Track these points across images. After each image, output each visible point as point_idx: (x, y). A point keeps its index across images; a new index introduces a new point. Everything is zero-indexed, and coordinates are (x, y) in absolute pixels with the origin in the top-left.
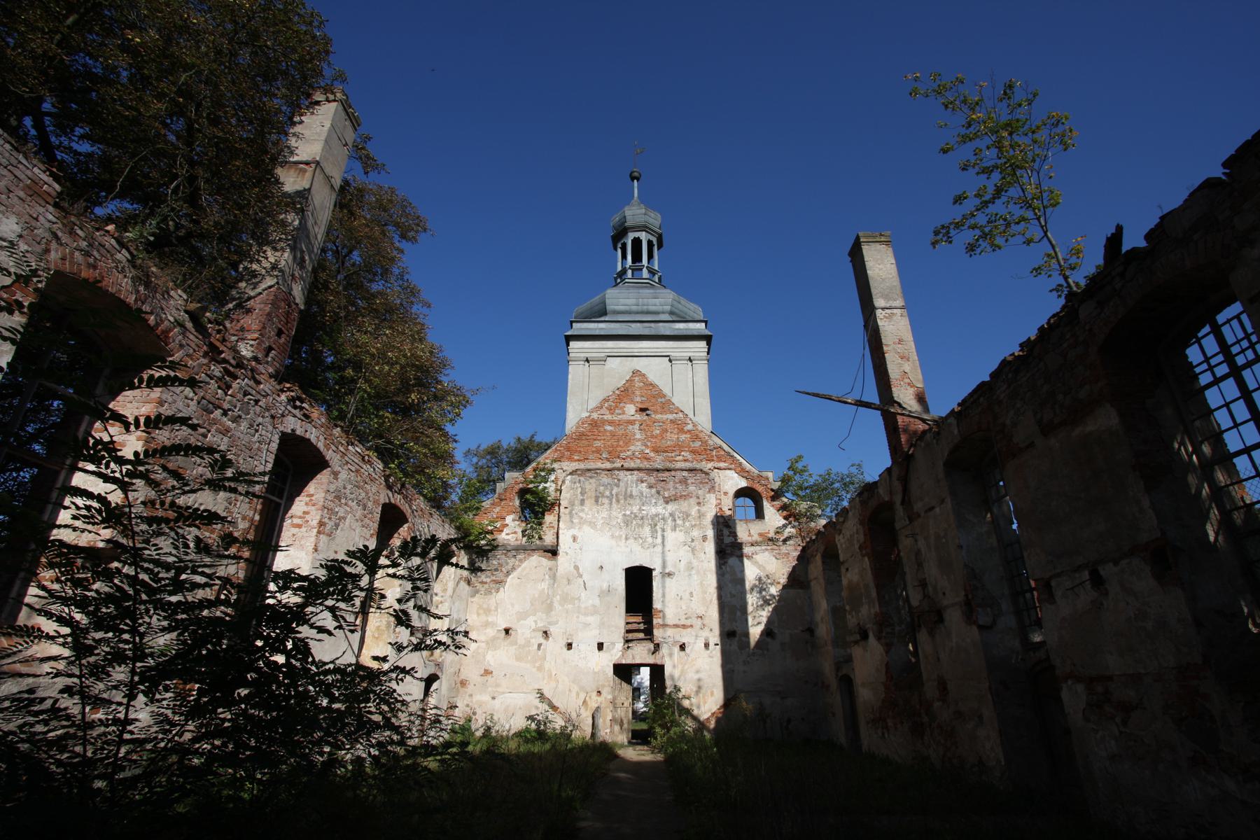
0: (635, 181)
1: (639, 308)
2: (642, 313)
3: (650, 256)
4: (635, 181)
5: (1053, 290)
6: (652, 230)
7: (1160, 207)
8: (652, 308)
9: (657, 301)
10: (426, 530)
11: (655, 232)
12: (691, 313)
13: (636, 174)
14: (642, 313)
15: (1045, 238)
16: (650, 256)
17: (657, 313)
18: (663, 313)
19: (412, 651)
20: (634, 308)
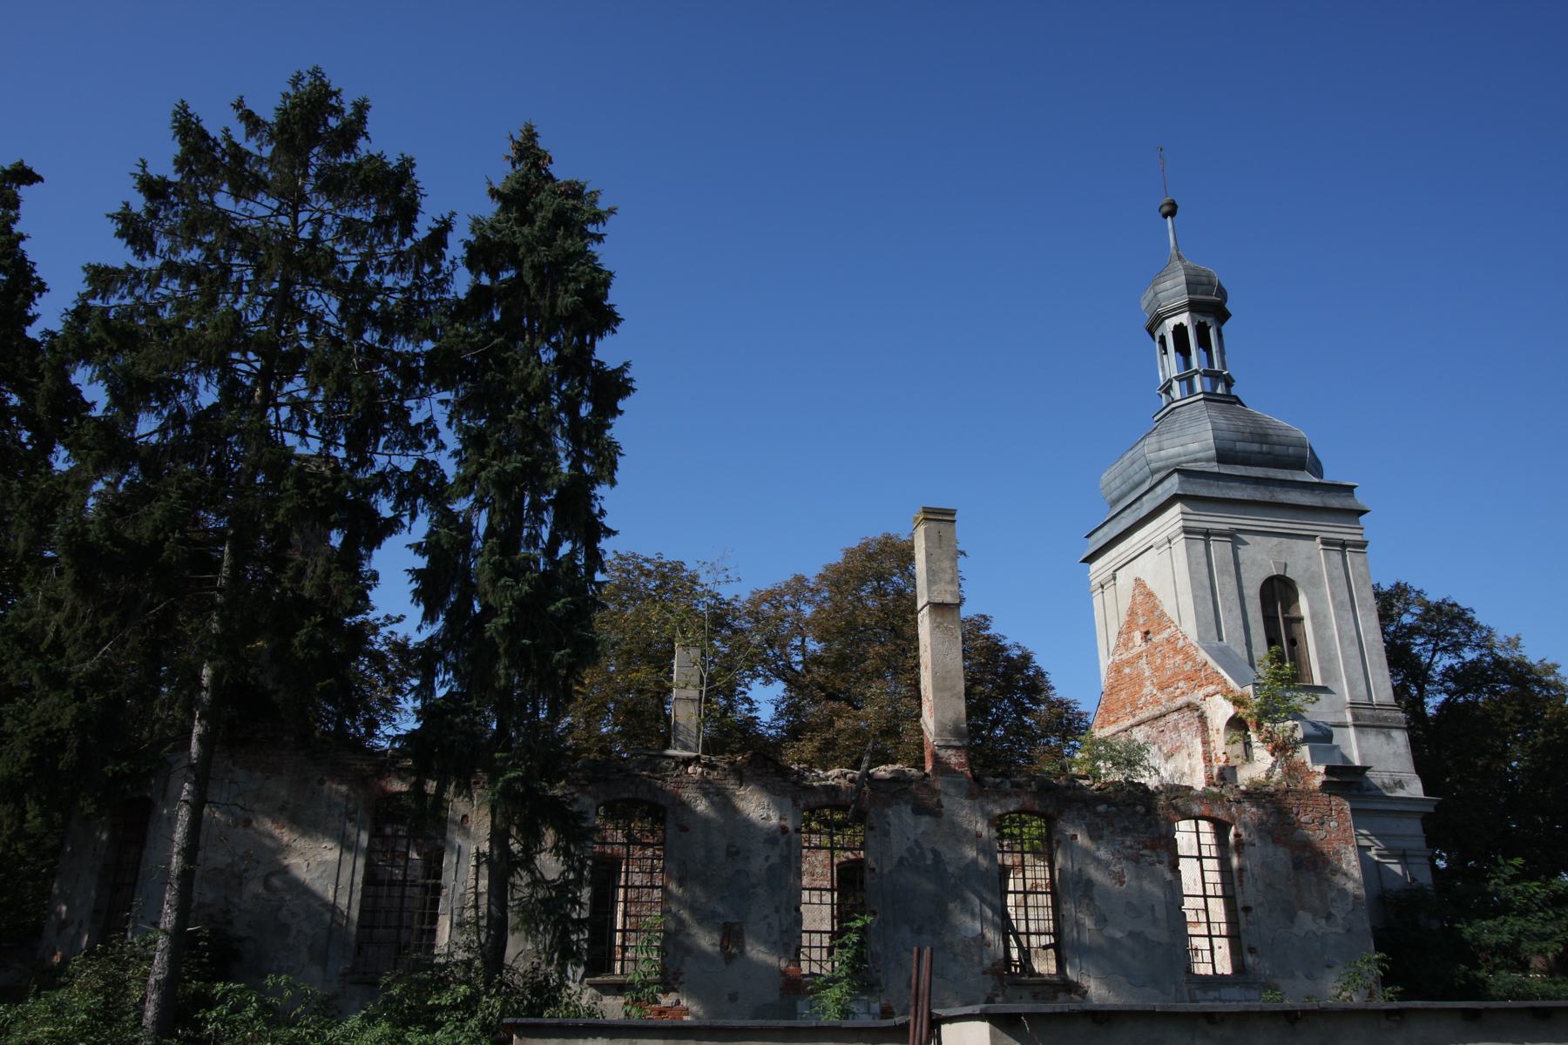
0: (1169, 218)
6: (1174, 309)
8: (1137, 478)
11: (1179, 308)
13: (1166, 209)
20: (1124, 488)
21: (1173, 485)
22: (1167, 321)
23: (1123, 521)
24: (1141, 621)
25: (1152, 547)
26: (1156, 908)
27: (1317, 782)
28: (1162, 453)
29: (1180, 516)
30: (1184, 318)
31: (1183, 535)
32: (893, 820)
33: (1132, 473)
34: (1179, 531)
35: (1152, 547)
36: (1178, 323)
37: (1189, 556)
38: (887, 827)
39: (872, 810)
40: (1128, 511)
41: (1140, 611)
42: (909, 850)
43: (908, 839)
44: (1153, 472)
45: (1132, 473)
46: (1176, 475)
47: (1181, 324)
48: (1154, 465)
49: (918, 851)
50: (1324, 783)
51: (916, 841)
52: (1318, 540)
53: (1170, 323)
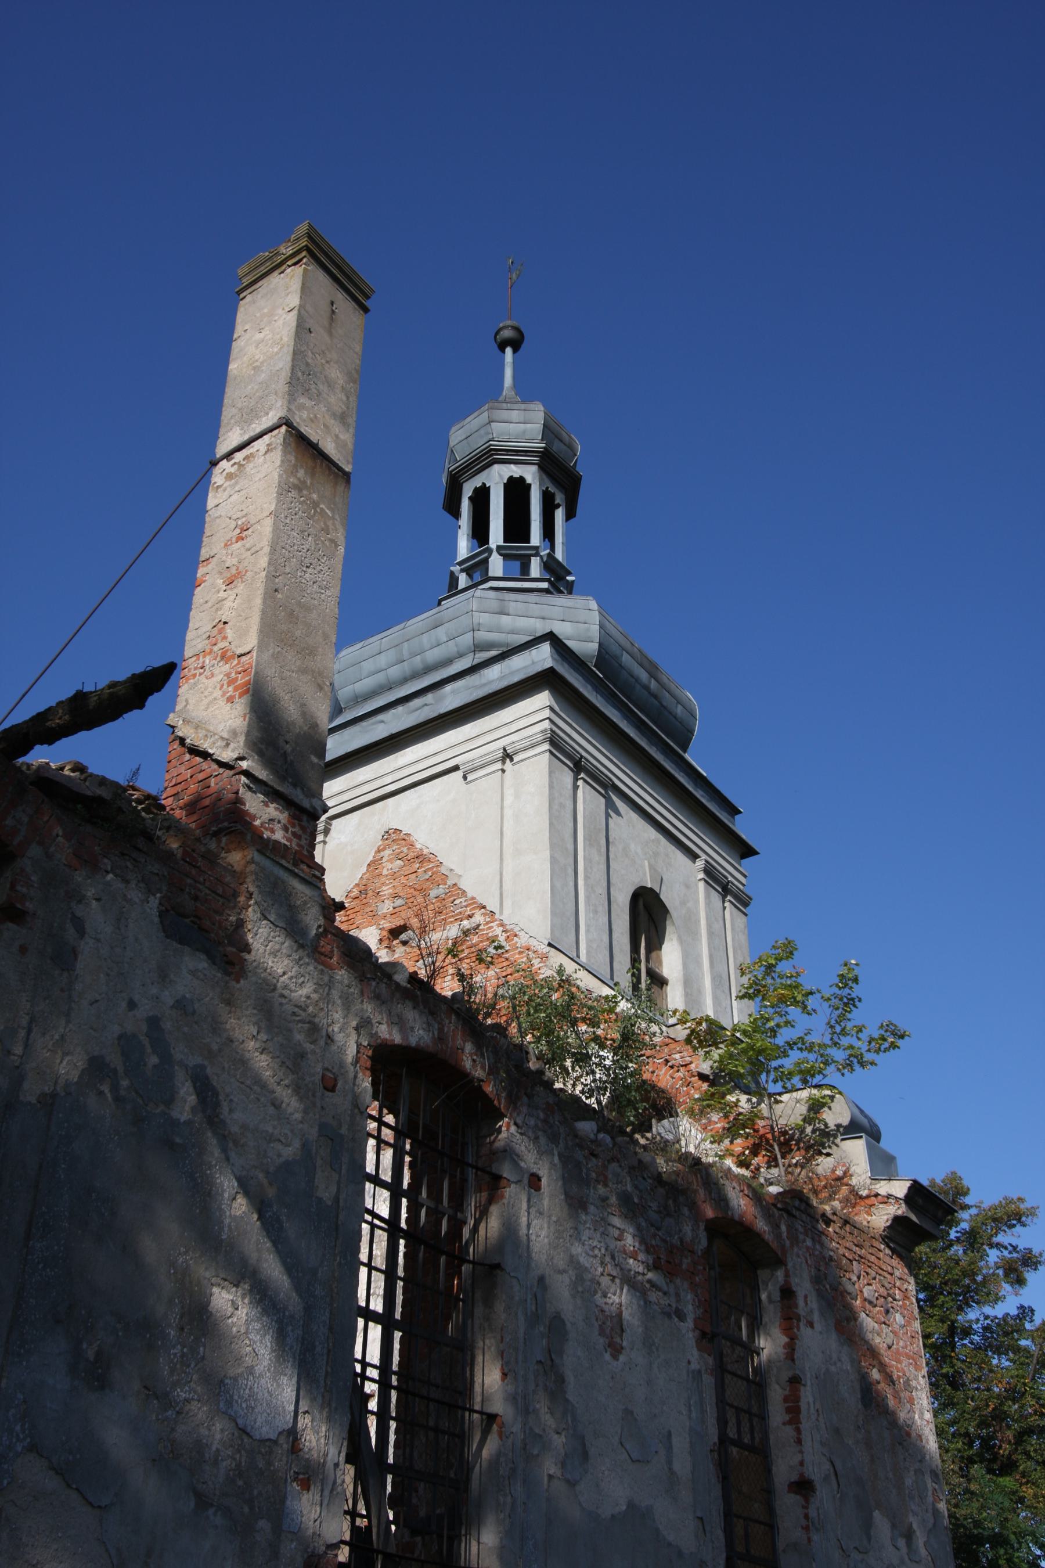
0: (509, 351)
1: (406, 668)
2: (415, 676)
3: (548, 532)
4: (509, 351)
5: (138, 769)
6: (517, 452)
7: (136, 773)
8: (433, 655)
9: (441, 633)
10: (803, 1173)
11: (526, 453)
12: (522, 623)
13: (507, 334)
14: (415, 676)
15: (728, 1378)
16: (548, 532)
17: (448, 662)
18: (461, 655)
19: (321, 905)
20: (395, 672)
21: (543, 657)
22: (496, 467)
23: (381, 726)
24: (386, 907)
25: (456, 768)
26: (675, 1441)
27: (880, 1218)
28: (505, 619)
29: (547, 713)
30: (530, 474)
31: (546, 746)
32: (94, 914)
33: (427, 646)
34: (540, 737)
35: (456, 768)
36: (516, 475)
37: (551, 787)
38: (71, 932)
39: (35, 851)
40: (400, 709)
41: (386, 890)
42: (126, 1042)
43: (132, 1005)
44: (478, 647)
45: (427, 646)
46: (546, 648)
47: (522, 479)
48: (483, 636)
49: (154, 1060)
50: (897, 1220)
51: (154, 1022)
52: (700, 863)
53: (496, 478)
